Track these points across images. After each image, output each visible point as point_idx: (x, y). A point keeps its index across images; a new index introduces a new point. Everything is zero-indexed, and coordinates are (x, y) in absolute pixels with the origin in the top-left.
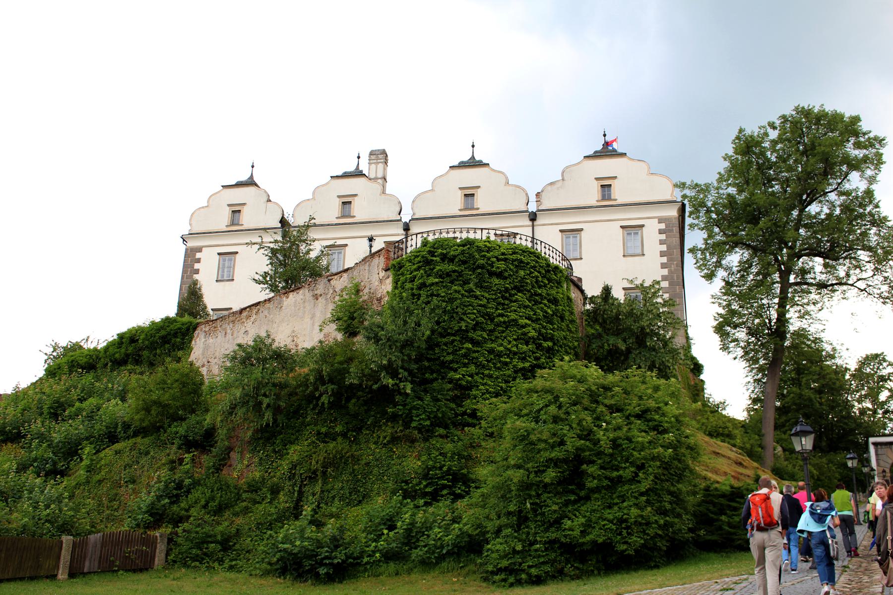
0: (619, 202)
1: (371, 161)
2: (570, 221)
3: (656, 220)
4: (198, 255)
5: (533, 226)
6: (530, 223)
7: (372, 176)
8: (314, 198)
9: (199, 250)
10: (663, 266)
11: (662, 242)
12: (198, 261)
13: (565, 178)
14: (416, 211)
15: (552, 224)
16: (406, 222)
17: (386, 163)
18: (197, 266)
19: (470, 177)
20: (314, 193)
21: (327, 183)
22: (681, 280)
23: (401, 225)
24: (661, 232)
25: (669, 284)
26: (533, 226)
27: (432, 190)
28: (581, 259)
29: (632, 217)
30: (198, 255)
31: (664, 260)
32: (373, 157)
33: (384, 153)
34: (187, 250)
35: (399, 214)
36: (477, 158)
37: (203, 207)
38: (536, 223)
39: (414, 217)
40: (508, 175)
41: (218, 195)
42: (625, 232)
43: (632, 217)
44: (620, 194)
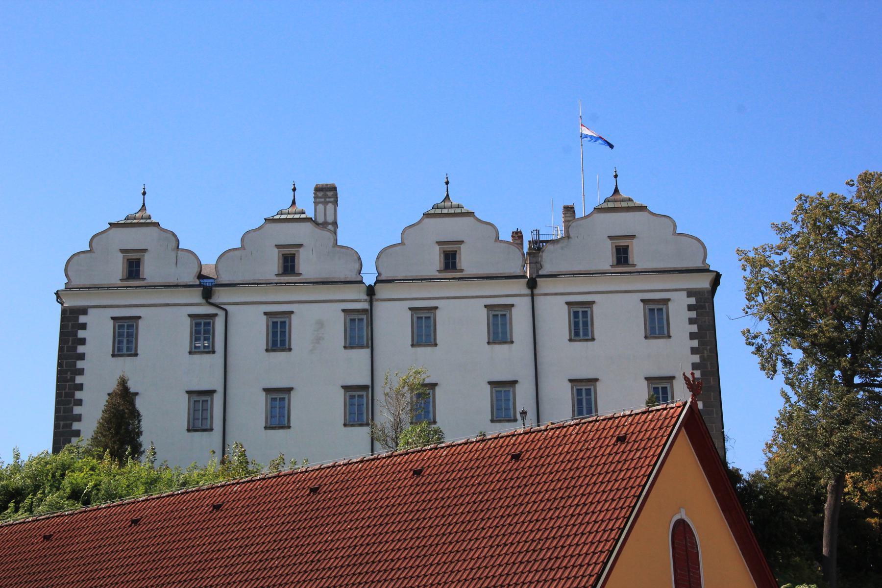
0: (640, 266)
1: (318, 200)
2: (579, 289)
3: (685, 293)
4: (82, 319)
5: (532, 296)
6: (528, 292)
7: (321, 220)
8: (243, 247)
9: (84, 311)
10: (694, 351)
11: (691, 321)
12: (84, 326)
13: (572, 235)
14: (382, 271)
15: (556, 294)
16: (370, 286)
17: (335, 202)
18: (81, 334)
19: (450, 229)
20: (242, 240)
21: (261, 227)
22: (719, 399)
23: (363, 289)
24: (690, 308)
25: (698, 329)
26: (532, 296)
27: (402, 244)
28: (289, 427)
29: (656, 286)
30: (82, 319)
31: (695, 343)
32: (320, 194)
33: (334, 189)
34: (64, 312)
35: (360, 273)
36: (454, 201)
37: (83, 252)
38: (536, 291)
39: (380, 278)
40: (497, 226)
41: (104, 235)
42: (415, 316)
43: (656, 286)
44: (639, 257)
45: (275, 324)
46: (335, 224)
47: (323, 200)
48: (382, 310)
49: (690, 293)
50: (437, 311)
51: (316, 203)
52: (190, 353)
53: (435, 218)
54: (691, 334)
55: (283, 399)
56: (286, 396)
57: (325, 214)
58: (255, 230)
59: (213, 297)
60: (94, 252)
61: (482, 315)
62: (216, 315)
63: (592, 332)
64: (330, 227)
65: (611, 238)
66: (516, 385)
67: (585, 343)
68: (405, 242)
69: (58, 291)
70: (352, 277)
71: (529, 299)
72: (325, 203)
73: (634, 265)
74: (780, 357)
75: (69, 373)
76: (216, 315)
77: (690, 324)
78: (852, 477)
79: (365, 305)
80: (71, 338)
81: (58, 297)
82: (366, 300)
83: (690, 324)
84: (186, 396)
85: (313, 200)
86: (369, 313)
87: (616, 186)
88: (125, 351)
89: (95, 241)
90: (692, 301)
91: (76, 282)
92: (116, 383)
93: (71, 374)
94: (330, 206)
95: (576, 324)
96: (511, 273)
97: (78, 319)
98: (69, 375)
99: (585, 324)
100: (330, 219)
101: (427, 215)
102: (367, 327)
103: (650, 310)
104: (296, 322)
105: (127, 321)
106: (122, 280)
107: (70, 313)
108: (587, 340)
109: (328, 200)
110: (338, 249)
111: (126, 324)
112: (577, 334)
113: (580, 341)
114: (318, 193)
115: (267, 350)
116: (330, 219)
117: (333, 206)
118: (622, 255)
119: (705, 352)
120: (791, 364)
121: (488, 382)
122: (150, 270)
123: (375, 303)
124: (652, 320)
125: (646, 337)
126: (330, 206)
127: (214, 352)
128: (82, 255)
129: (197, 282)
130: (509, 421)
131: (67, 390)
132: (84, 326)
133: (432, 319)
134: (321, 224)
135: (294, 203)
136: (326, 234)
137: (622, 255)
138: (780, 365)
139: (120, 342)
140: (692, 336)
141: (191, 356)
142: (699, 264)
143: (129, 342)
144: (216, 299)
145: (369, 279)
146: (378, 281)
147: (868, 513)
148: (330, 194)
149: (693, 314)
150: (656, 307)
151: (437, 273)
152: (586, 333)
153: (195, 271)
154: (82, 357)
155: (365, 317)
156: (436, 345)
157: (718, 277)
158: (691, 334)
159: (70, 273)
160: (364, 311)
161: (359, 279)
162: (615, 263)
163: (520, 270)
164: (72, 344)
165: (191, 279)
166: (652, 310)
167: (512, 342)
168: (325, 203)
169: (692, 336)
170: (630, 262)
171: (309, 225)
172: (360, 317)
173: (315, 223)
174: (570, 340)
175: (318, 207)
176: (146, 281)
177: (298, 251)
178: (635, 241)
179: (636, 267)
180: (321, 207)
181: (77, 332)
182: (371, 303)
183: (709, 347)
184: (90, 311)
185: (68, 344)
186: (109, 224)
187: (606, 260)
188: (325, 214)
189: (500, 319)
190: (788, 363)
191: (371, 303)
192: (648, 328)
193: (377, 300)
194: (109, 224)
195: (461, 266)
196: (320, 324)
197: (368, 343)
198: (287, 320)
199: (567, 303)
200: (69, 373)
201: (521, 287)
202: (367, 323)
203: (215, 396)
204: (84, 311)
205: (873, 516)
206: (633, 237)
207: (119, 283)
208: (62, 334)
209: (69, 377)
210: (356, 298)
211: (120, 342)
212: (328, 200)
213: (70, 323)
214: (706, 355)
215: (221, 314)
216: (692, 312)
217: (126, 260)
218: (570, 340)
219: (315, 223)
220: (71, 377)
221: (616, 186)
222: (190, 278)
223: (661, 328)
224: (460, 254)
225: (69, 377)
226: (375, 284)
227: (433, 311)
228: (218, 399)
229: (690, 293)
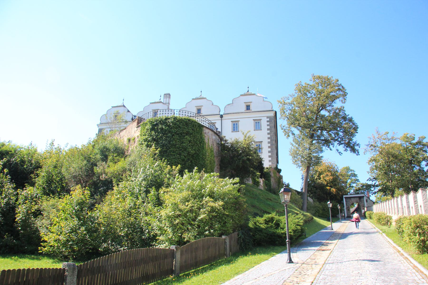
0: (253, 110)
2: (235, 117)
3: (266, 117)
6: (221, 119)
7: (165, 102)
21: (149, 105)
24: (267, 121)
27: (186, 107)
32: (165, 96)
33: (169, 94)
34: (99, 129)
38: (222, 118)
43: (257, 116)
44: (252, 108)
45: (234, 124)
46: (169, 103)
49: (267, 117)
51: (164, 98)
55: (259, 122)
56: (260, 122)
57: (166, 101)
58: (147, 106)
63: (239, 129)
64: (167, 104)
67: (236, 133)
73: (251, 110)
74: (291, 132)
78: (323, 176)
90: (268, 119)
94: (168, 99)
95: (234, 127)
99: (237, 127)
103: (256, 122)
104: (240, 124)
108: (237, 132)
112: (234, 130)
113: (235, 132)
118: (248, 107)
120: (294, 134)
124: (256, 125)
125: (254, 130)
126: (168, 99)
133: (260, 123)
135: (160, 99)
137: (248, 107)
138: (290, 134)
140: (268, 129)
142: (270, 109)
147: (327, 185)
148: (168, 95)
149: (268, 123)
152: (237, 130)
156: (261, 130)
157: (276, 112)
159: (101, 120)
166: (256, 123)
168: (166, 98)
169: (268, 129)
170: (250, 109)
171: (161, 104)
172: (259, 121)
174: (232, 132)
178: (252, 103)
187: (244, 109)
188: (166, 101)
190: (293, 134)
192: (255, 128)
198: (238, 123)
199: (231, 121)
201: (218, 117)
205: (328, 186)
206: (251, 102)
218: (232, 132)
223: (259, 128)
229: (267, 117)
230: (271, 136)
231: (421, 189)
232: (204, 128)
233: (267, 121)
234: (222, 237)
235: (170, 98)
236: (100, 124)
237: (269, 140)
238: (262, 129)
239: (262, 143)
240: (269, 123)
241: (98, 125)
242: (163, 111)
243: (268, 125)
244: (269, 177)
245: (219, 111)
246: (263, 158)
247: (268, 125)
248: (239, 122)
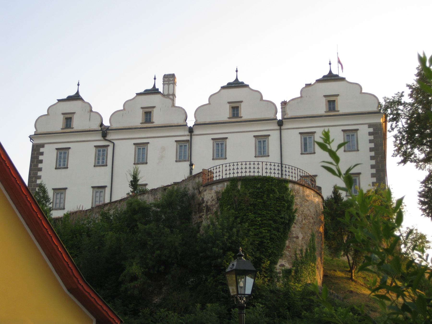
3: (367, 126)
4: (42, 150)
5: (280, 130)
7: (166, 93)
8: (124, 109)
9: (42, 146)
12: (42, 154)
16: (190, 127)
18: (41, 158)
24: (370, 134)
26: (280, 130)
30: (42, 150)
32: (166, 79)
33: (173, 76)
34: (33, 146)
42: (345, 134)
46: (174, 95)
47: (167, 82)
48: (195, 139)
49: (370, 126)
50: (227, 140)
51: (164, 84)
52: (94, 166)
53: (73, 101)
54: (370, 148)
57: (168, 90)
58: (130, 100)
59: (107, 136)
60: (172, 107)
61: (253, 141)
62: (108, 146)
64: (171, 97)
65: (325, 96)
66: (67, 190)
68: (211, 103)
69: (30, 136)
70: (181, 122)
71: (279, 131)
72: (169, 84)
75: (34, 178)
76: (108, 146)
77: (370, 143)
79: (188, 138)
80: (36, 160)
81: (31, 139)
82: (188, 135)
83: (370, 143)
84: (92, 189)
85: (162, 82)
86: (190, 142)
87: (237, 76)
88: (62, 166)
89: (50, 109)
90: (371, 130)
91: (40, 131)
92: (407, 163)
93: (35, 179)
96: (269, 118)
97: (374, 129)
98: (34, 179)
100: (171, 92)
101: (223, 88)
102: (189, 150)
105: (64, 150)
106: (62, 129)
107: (36, 147)
109: (170, 82)
110: (175, 108)
111: (63, 152)
113: (307, 154)
114: (165, 79)
115: (176, 161)
116: (171, 92)
117: (173, 85)
119: (378, 158)
121: (52, 189)
122: (77, 124)
123: (193, 137)
126: (171, 86)
127: (106, 165)
128: (43, 117)
129: (100, 129)
130: (61, 209)
131: (33, 187)
132: (42, 154)
134: (166, 95)
136: (168, 101)
139: (99, 159)
141: (95, 168)
143: (64, 161)
144: (109, 137)
145: (191, 123)
146: (195, 125)
148: (171, 79)
149: (372, 137)
150: (101, 149)
151: (228, 119)
153: (99, 123)
154: (40, 170)
155: (187, 144)
156: (358, 150)
158: (370, 148)
160: (187, 141)
161: (185, 124)
162: (328, 110)
163: (274, 115)
164: (36, 163)
165: (96, 126)
167: (269, 156)
168: (169, 84)
169: (371, 150)
170: (336, 109)
173: (163, 95)
174: (302, 154)
175: (165, 86)
176: (154, 124)
177: (241, 104)
178: (339, 98)
179: (74, 129)
180: (166, 86)
181: (39, 157)
182: (191, 136)
183: (380, 156)
184: (46, 145)
185: (34, 163)
186: (58, 100)
188: (168, 90)
189: (351, 137)
191: (191, 136)
193: (194, 135)
194: (58, 100)
195: (241, 115)
196: (163, 149)
197: (188, 158)
200: (34, 178)
202: (189, 148)
203: (106, 189)
204: (42, 146)
207: (139, 125)
208: (32, 158)
209: (34, 180)
210: (183, 135)
211: (99, 159)
212: (170, 82)
213: (36, 152)
214: (378, 160)
215: (111, 145)
216: (371, 136)
217: (144, 113)
218: (302, 154)
219: (163, 95)
220: (35, 180)
221: (237, 76)
222: (96, 126)
224: (241, 108)
225: (34, 180)
226: (193, 126)
227: (225, 140)
228: (108, 190)
229: (370, 126)
230: (377, 162)
231: (46, 214)
232: (290, 186)
233: (370, 134)
234: (339, 258)
235: (174, 83)
236: (35, 135)
237: (372, 170)
238: (359, 149)
239: (361, 176)
240: (373, 136)
241: (31, 137)
242: (242, 164)
243: (371, 141)
244: (105, 216)
245: (274, 112)
246: (410, 87)
247: (371, 141)
248: (315, 134)
